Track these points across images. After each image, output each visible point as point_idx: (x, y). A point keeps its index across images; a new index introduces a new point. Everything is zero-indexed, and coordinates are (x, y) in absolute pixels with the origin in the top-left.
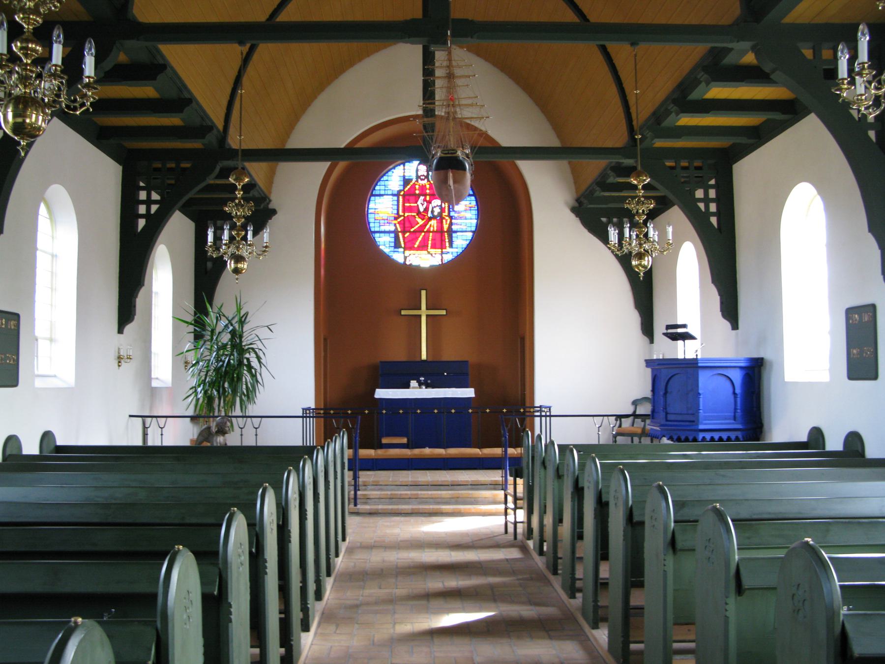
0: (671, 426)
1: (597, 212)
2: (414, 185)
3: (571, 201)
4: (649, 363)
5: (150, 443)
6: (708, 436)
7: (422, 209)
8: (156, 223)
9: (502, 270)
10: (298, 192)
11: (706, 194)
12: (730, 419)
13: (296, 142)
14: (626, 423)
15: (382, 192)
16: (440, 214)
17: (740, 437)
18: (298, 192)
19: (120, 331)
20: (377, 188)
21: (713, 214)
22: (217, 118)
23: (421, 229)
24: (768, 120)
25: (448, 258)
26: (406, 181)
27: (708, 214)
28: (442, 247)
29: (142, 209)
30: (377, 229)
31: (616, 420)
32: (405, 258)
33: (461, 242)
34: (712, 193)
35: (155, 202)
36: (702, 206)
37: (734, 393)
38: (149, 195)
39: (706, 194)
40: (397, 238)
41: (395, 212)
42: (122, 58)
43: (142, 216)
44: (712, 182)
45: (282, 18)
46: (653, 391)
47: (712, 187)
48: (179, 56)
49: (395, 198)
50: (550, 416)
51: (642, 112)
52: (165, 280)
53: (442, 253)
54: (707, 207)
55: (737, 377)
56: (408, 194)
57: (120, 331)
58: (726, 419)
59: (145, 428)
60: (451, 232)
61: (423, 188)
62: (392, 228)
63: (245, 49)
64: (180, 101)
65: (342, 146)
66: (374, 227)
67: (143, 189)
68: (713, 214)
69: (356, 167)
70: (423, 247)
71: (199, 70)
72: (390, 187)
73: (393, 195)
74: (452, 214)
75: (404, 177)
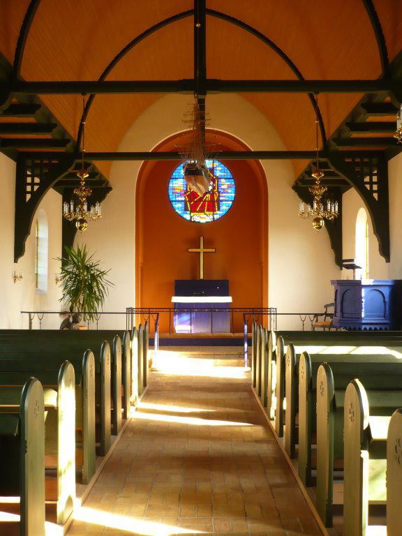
1: (303, 190)
3: (293, 182)
4: (333, 282)
5: (33, 328)
6: (368, 327)
8: (37, 197)
9: (248, 226)
10: (125, 180)
11: (371, 179)
14: (321, 319)
15: (177, 177)
17: (388, 328)
18: (125, 180)
19: (16, 261)
20: (174, 174)
21: (375, 192)
22: (72, 133)
23: (201, 199)
25: (217, 217)
27: (372, 191)
28: (214, 210)
29: (29, 188)
30: (174, 199)
31: (314, 317)
32: (191, 217)
33: (225, 207)
34: (375, 179)
35: (37, 184)
36: (368, 187)
37: (384, 301)
38: (33, 180)
39: (371, 179)
40: (186, 205)
41: (185, 189)
42: (14, 100)
43: (29, 193)
44: (375, 172)
45: (108, 78)
46: (335, 300)
47: (375, 175)
48: (46, 99)
50: (276, 314)
51: (331, 130)
52: (46, 232)
54: (371, 187)
55: (386, 291)
56: (71, 217)
57: (16, 261)
59: (30, 320)
60: (219, 201)
62: (183, 199)
63: (87, 97)
64: (49, 124)
65: (150, 151)
66: (172, 197)
67: (29, 176)
68: (375, 192)
69: (159, 164)
70: (202, 210)
71: (62, 108)
74: (220, 190)
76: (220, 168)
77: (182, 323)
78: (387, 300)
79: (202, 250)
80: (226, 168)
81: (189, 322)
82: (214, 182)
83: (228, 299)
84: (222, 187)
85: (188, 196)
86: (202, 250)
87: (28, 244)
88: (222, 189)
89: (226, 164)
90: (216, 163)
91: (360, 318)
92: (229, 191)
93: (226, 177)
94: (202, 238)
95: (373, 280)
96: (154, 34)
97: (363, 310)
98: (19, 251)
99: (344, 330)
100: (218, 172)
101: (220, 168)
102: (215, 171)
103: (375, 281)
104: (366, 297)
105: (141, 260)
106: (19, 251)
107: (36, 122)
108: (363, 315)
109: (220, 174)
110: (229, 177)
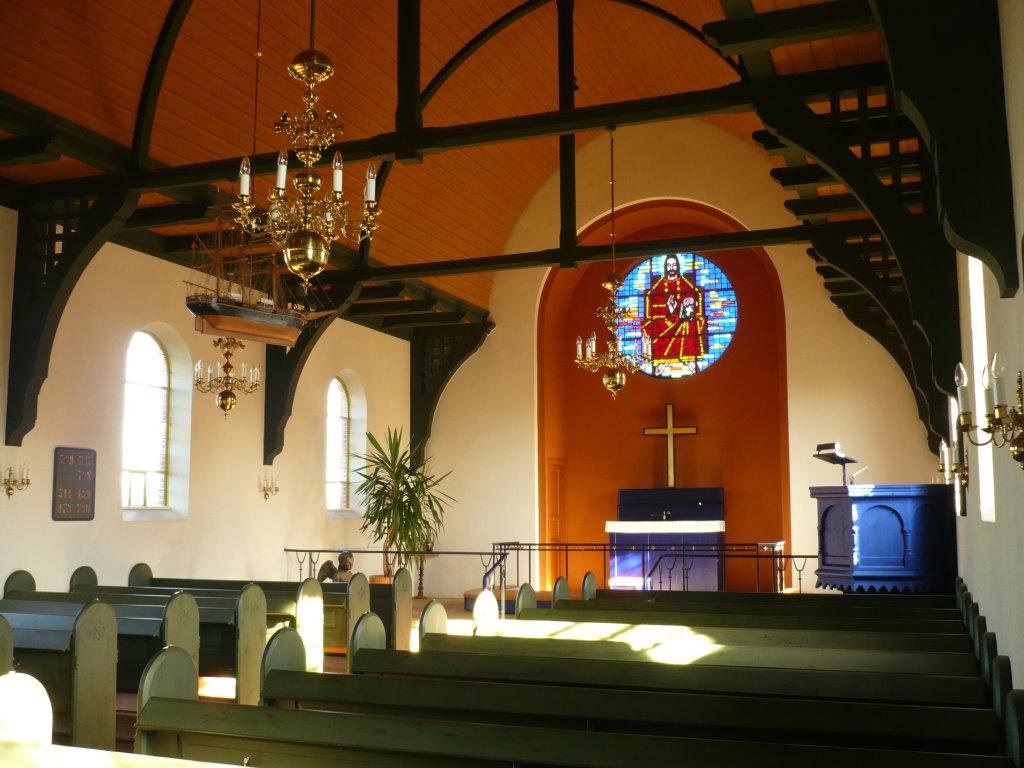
0: (832, 571)
2: (663, 281)
7: (671, 310)
9: (756, 378)
10: (518, 303)
12: (898, 564)
13: (513, 248)
15: (627, 293)
16: (694, 314)
18: (518, 303)
24: (851, 194)
25: (702, 365)
26: (654, 278)
28: (697, 353)
32: (654, 368)
33: (719, 344)
37: (903, 531)
41: (642, 315)
49: (642, 299)
53: (697, 360)
55: (908, 510)
57: (268, 459)
58: (892, 564)
60: (706, 335)
61: (672, 285)
70: (674, 354)
72: (635, 287)
73: (639, 295)
74: (707, 313)
75: (651, 273)
76: (706, 271)
77: (626, 572)
78: (909, 526)
79: (670, 430)
80: (718, 270)
81: (641, 569)
82: (696, 299)
83: (715, 526)
84: (712, 307)
85: (647, 328)
86: (670, 430)
87: (292, 429)
88: (712, 311)
89: (711, 258)
90: (700, 262)
91: (849, 566)
92: (726, 314)
93: (719, 287)
94: (670, 409)
95: (873, 486)
96: (492, 43)
97: (856, 549)
98: (272, 445)
99: (841, 592)
100: (703, 277)
101: (706, 271)
102: (698, 278)
103: (877, 488)
104: (861, 522)
105: (553, 452)
106: (272, 445)
107: (798, 197)
108: (856, 560)
109: (708, 281)
110: (724, 286)
